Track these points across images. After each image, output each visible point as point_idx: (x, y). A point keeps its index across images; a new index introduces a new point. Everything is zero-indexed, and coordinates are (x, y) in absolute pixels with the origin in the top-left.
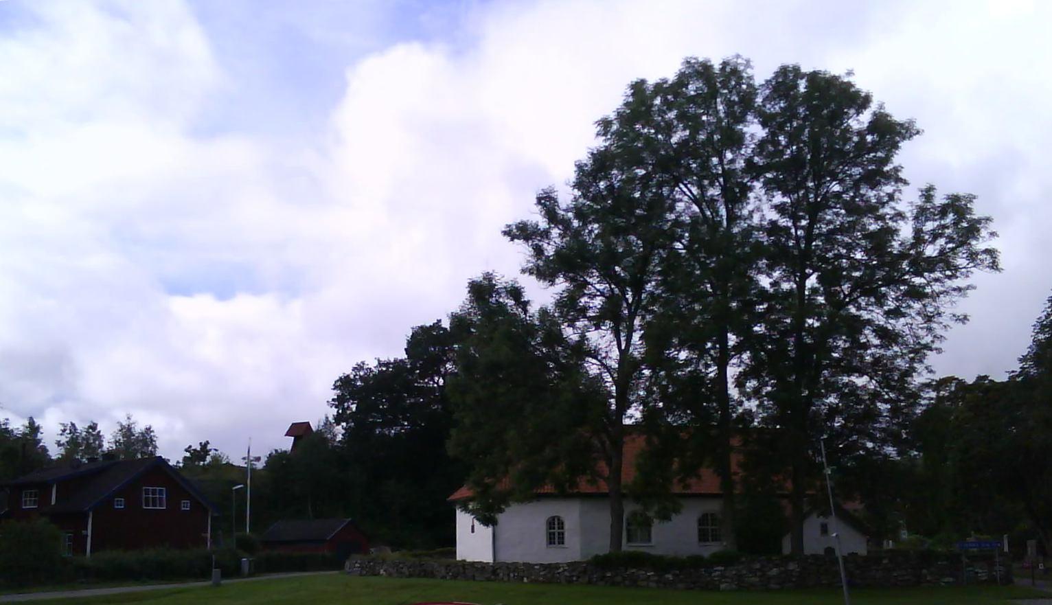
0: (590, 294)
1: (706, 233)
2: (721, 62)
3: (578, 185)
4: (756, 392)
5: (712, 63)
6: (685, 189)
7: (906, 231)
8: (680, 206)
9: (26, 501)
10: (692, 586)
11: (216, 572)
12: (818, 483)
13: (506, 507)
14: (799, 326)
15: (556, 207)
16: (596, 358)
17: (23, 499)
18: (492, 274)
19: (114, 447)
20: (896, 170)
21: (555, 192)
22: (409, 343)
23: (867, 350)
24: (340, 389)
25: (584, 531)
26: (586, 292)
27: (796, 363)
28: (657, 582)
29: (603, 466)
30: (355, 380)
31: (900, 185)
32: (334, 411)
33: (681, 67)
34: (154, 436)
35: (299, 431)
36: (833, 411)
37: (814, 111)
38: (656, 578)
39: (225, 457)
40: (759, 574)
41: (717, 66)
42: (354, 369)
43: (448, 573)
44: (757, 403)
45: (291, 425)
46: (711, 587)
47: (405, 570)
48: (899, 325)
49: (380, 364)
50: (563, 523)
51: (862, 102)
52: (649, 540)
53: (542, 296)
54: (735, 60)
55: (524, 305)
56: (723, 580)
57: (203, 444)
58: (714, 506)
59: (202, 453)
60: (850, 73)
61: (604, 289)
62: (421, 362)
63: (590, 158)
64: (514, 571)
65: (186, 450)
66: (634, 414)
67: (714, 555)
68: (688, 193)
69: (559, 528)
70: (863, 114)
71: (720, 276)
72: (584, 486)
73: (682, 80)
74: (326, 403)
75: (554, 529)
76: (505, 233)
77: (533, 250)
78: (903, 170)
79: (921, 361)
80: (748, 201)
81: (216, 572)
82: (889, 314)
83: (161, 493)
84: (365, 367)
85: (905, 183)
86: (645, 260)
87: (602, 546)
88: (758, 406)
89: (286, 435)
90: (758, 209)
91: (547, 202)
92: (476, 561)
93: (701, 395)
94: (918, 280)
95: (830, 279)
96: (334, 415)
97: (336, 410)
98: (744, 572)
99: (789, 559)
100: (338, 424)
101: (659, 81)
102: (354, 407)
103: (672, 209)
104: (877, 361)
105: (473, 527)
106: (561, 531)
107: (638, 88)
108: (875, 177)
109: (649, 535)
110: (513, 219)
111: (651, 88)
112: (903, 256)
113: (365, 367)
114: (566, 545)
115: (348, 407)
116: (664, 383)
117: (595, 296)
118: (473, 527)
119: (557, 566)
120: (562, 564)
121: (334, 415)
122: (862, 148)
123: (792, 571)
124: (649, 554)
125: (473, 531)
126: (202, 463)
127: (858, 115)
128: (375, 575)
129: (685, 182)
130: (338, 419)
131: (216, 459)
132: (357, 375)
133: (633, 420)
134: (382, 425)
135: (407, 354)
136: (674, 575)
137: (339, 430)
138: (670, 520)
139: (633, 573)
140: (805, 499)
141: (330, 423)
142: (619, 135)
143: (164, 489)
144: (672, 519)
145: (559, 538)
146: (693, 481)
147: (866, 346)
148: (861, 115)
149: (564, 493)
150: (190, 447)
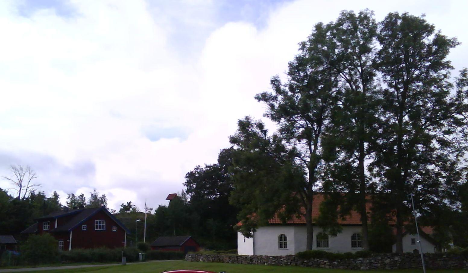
0: (297, 127)
1: (354, 98)
2: (359, 12)
3: (290, 74)
4: (378, 174)
5: (354, 13)
6: (343, 76)
7: (453, 93)
8: (340, 84)
9: (45, 227)
10: (347, 267)
11: (124, 259)
13: (257, 229)
14: (399, 141)
15: (280, 85)
16: (299, 157)
17: (44, 226)
18: (249, 117)
20: (448, 62)
21: (279, 77)
22: (219, 157)
23: (433, 152)
24: (189, 178)
25: (295, 241)
26: (295, 126)
27: (399, 158)
28: (329, 265)
29: (303, 210)
31: (450, 69)
32: (186, 188)
33: (339, 16)
34: (106, 199)
35: (172, 198)
36: (417, 182)
37: (405, 35)
38: (329, 263)
39: (137, 208)
40: (380, 262)
41: (357, 15)
42: (195, 169)
43: (230, 260)
44: (379, 179)
45: (168, 195)
46: (357, 268)
47: (211, 259)
48: (449, 138)
49: (207, 167)
50: (286, 238)
51: (429, 29)
52: (328, 246)
53: (273, 128)
54: (366, 11)
55: (265, 132)
56: (362, 265)
57: (129, 203)
58: (359, 230)
60: (424, 15)
61: (303, 124)
62: (225, 165)
63: (295, 60)
65: (121, 206)
66: (319, 184)
67: (358, 253)
68: (344, 77)
69: (284, 240)
70: (430, 36)
71: (360, 117)
73: (341, 22)
74: (182, 184)
75: (282, 240)
76: (256, 98)
77: (270, 107)
78: (451, 63)
79: (462, 156)
80: (374, 81)
81: (124, 259)
82: (446, 133)
83: (103, 223)
84: (200, 168)
85: (453, 68)
86: (322, 110)
88: (380, 181)
89: (166, 199)
90: (379, 85)
91: (275, 83)
92: (243, 255)
93: (349, 175)
94: (459, 117)
95: (415, 117)
96: (186, 190)
97: (187, 187)
98: (373, 261)
99: (396, 254)
101: (329, 23)
102: (194, 186)
103: (336, 86)
106: (285, 241)
107: (319, 27)
108: (437, 65)
109: (328, 244)
110: (260, 91)
111: (325, 27)
112: (452, 105)
113: (200, 168)
114: (288, 248)
115: (192, 186)
117: (299, 128)
118: (245, 239)
119: (281, 257)
121: (186, 190)
122: (429, 52)
123: (397, 261)
124: (325, 252)
125: (245, 242)
126: (128, 211)
127: (428, 37)
128: (199, 261)
129: (343, 72)
130: (188, 192)
131: (134, 210)
132: (196, 171)
133: (318, 187)
135: (218, 162)
136: (338, 262)
137: (188, 198)
138: (337, 236)
139: (318, 261)
141: (184, 193)
142: (310, 50)
144: (337, 235)
145: (284, 245)
146: (348, 217)
147: (433, 150)
148: (429, 36)
149: (284, 224)
150: (123, 204)
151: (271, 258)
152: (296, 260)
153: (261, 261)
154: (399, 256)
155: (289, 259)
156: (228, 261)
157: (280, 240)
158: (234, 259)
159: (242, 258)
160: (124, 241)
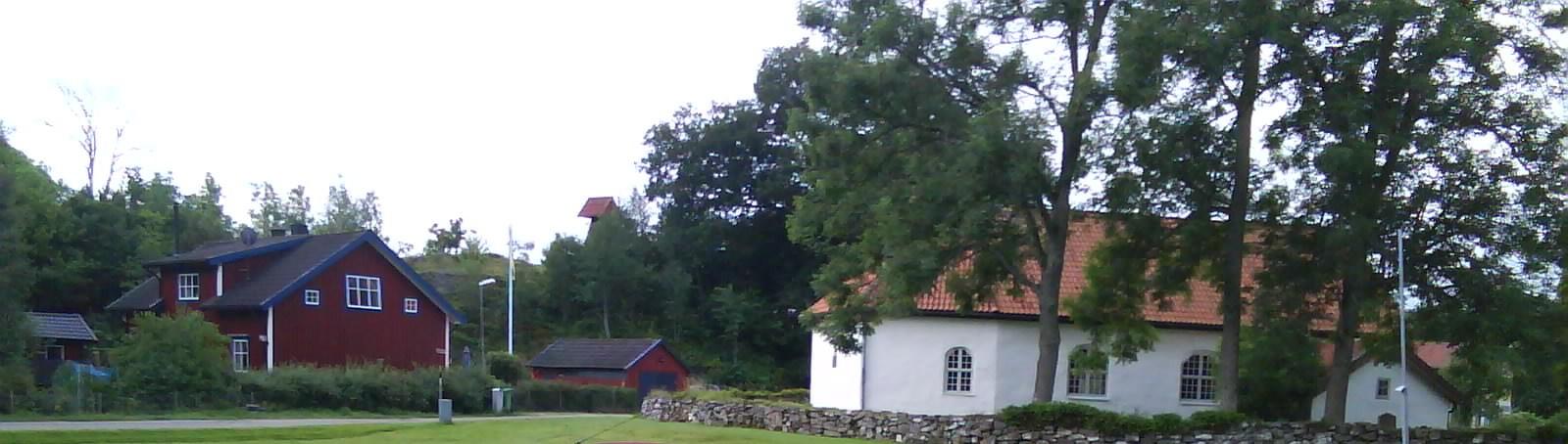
4: (1298, 160)
11: (445, 404)
12: (1383, 313)
16: (1034, 86)
19: (327, 222)
25: (1001, 369)
29: (1033, 269)
30: (677, 131)
35: (600, 211)
36: (1424, 194)
43: (784, 423)
47: (723, 416)
50: (970, 359)
57: (454, 222)
59: (454, 236)
64: (882, 425)
66: (1089, 190)
67: (1198, 416)
72: (1007, 304)
81: (445, 404)
83: (374, 285)
87: (1024, 395)
89: (580, 215)
99: (1322, 427)
100: (651, 199)
102: (674, 174)
104: (1514, 110)
105: (835, 358)
106: (966, 370)
116: (1147, 136)
118: (835, 358)
119: (949, 420)
120: (956, 417)
125: (834, 365)
130: (653, 191)
131: (473, 246)
134: (717, 204)
138: (1136, 360)
139: (1067, 436)
140: (1356, 340)
143: (378, 279)
146: (1177, 299)
151: (919, 420)
152: (995, 432)
153: (885, 429)
154: (1330, 433)
155: (978, 427)
156: (780, 424)
157: (950, 366)
158: (797, 418)
159: (824, 416)
160: (444, 348)
